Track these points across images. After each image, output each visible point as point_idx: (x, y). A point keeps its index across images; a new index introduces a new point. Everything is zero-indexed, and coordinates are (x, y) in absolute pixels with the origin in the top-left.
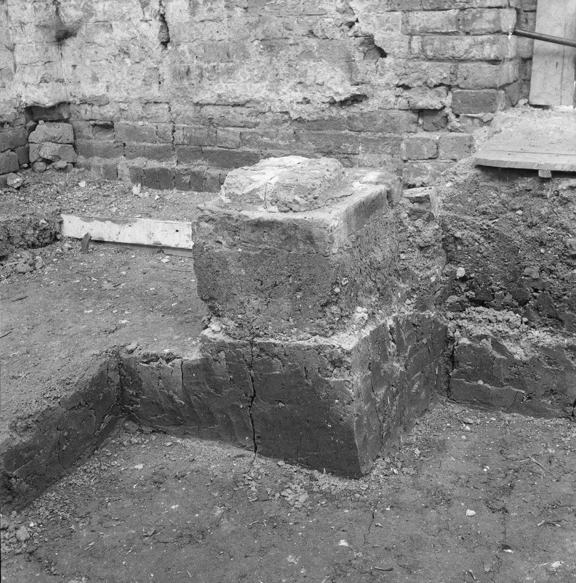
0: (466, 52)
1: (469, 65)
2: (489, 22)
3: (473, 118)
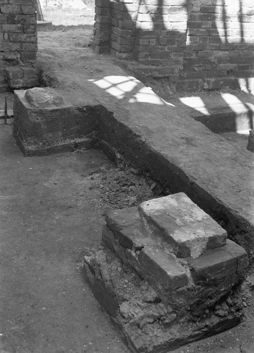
0: (25, 39)
1: (27, 44)
2: (32, 29)
3: (28, 62)
